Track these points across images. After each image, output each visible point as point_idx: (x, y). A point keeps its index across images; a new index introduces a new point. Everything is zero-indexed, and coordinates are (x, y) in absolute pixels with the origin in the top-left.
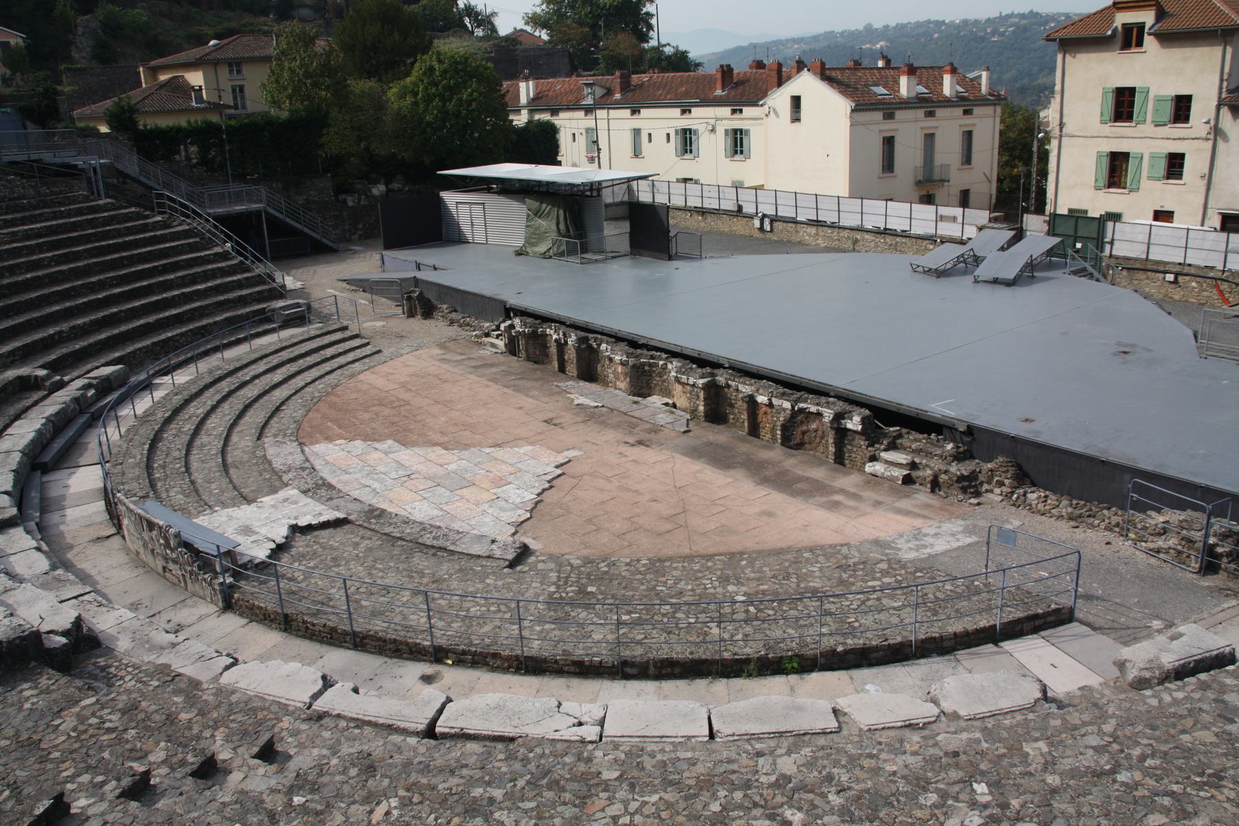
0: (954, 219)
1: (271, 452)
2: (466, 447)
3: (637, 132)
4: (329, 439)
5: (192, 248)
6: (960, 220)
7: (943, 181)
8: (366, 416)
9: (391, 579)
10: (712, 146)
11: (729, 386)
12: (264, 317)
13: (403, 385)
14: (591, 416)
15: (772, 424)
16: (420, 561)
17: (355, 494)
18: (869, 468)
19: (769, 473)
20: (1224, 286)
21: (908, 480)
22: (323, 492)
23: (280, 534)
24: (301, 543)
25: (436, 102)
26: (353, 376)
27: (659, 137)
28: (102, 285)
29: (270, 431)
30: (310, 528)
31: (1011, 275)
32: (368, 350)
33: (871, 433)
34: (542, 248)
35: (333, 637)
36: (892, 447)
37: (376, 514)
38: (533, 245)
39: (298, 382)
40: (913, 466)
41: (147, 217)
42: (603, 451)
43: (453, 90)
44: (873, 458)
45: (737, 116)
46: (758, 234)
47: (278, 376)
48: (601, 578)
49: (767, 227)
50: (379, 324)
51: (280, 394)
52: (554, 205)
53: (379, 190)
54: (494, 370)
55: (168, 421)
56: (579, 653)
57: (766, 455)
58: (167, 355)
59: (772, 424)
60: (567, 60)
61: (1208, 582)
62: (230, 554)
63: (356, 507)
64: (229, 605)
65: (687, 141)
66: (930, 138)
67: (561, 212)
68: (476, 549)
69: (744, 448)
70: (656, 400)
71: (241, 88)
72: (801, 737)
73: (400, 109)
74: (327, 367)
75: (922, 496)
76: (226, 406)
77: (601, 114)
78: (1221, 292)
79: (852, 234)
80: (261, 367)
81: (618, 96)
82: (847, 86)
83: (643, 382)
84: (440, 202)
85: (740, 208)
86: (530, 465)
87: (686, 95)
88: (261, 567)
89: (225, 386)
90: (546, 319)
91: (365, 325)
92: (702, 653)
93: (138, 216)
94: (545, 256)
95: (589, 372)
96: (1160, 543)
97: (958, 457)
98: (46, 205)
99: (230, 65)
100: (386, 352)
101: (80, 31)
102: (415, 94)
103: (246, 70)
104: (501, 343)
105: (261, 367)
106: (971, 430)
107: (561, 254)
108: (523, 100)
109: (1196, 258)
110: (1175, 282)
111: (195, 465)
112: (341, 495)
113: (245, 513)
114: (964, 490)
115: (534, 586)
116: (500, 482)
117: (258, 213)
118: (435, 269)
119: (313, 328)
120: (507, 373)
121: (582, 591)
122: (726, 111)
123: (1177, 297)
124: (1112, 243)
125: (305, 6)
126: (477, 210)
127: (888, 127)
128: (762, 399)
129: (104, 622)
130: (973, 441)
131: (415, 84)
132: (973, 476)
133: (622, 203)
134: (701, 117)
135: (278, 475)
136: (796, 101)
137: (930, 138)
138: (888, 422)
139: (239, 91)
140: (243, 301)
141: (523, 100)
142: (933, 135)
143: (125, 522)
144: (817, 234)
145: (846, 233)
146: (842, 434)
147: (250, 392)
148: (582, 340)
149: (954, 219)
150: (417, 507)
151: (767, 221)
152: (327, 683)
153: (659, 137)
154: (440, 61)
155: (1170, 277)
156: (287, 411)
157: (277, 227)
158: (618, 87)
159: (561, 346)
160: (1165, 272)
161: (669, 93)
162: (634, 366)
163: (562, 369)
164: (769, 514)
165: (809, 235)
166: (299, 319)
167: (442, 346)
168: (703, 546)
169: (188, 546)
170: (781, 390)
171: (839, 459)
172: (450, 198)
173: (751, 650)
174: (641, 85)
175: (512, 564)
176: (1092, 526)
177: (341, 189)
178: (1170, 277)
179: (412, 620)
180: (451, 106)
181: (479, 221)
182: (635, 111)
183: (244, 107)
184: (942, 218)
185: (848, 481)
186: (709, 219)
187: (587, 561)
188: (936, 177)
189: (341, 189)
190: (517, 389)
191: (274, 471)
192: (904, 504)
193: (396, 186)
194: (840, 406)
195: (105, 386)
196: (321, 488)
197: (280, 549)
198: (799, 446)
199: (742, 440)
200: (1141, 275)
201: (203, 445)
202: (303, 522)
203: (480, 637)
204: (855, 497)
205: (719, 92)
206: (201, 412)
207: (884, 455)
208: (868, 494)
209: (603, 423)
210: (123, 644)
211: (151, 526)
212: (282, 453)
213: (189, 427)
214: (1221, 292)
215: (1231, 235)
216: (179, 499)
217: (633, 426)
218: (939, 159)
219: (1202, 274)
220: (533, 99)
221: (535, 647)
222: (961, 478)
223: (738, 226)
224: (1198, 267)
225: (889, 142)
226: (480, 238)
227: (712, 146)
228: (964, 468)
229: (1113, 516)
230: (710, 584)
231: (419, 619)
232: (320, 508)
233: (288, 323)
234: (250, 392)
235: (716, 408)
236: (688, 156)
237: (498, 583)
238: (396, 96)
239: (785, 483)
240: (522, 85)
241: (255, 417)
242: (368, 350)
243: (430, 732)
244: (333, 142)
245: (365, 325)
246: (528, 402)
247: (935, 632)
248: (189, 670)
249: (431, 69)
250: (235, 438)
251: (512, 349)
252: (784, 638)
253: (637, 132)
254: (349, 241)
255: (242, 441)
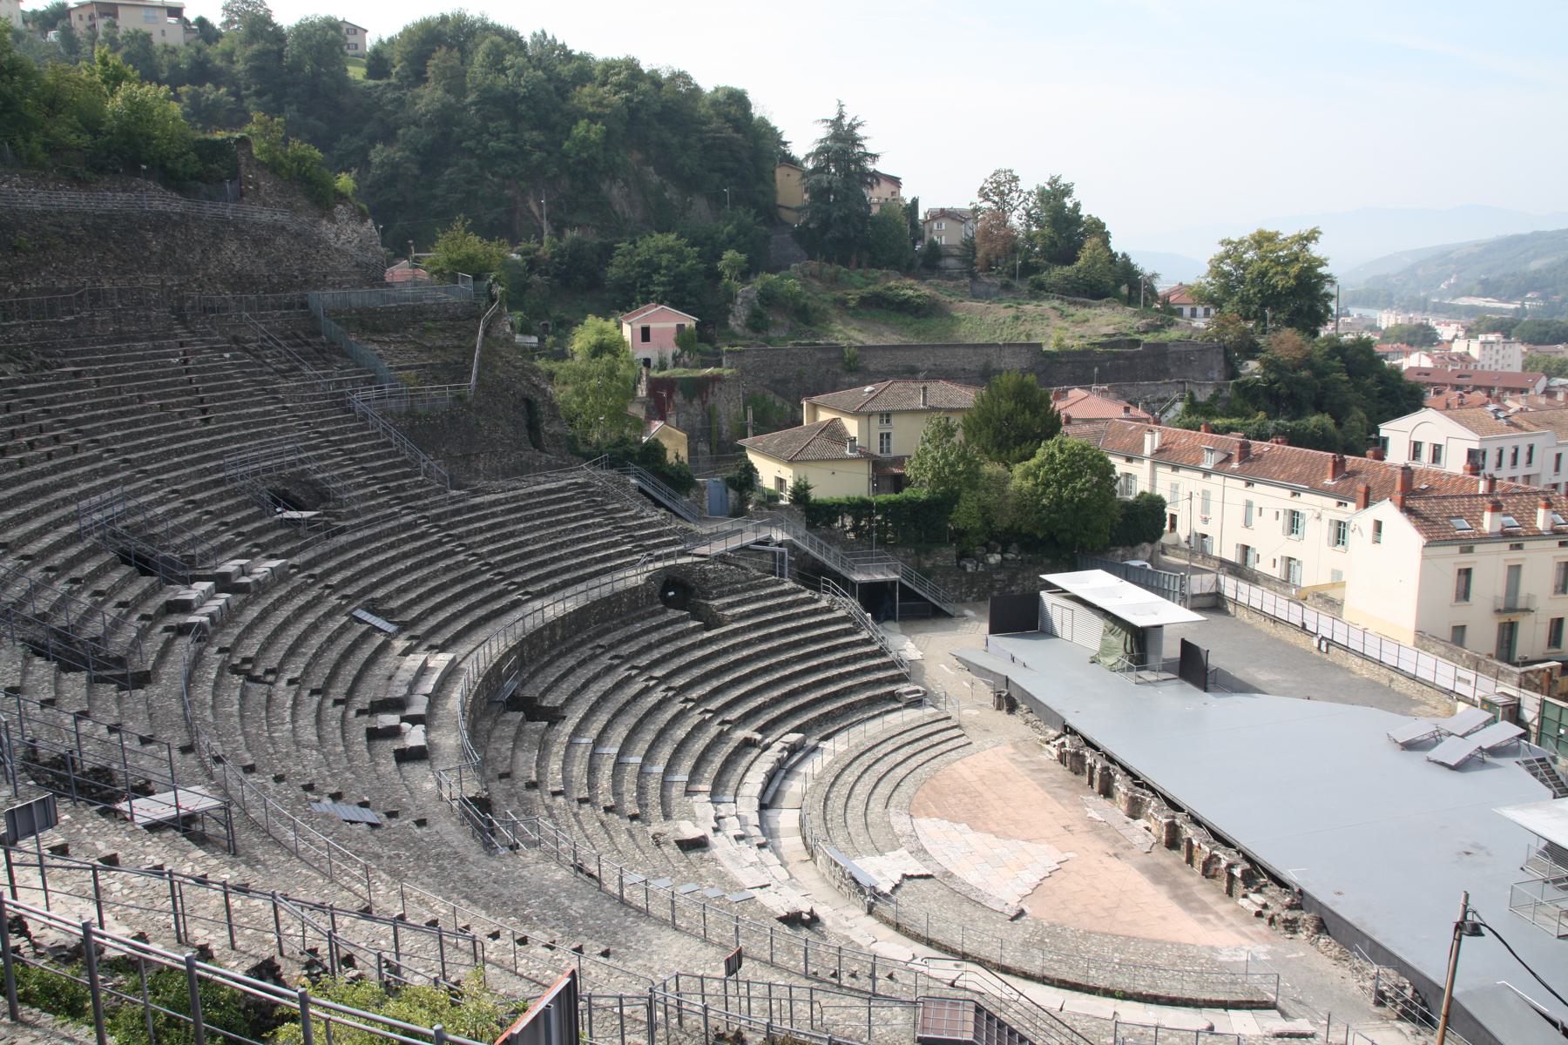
0: (1469, 682)
1: (893, 819)
2: (1010, 837)
3: (1249, 505)
4: (928, 815)
5: (847, 632)
7: (1527, 610)
8: (953, 801)
9: (950, 915)
10: (1316, 532)
12: (893, 697)
13: (981, 778)
14: (1095, 828)
15: (1200, 858)
16: (966, 907)
17: (939, 859)
19: (1180, 892)
21: (1259, 914)
22: (921, 855)
23: (897, 878)
24: (907, 884)
25: (1053, 488)
26: (949, 763)
27: (1269, 514)
28: (787, 663)
29: (893, 802)
30: (911, 877)
31: (1453, 763)
32: (962, 741)
33: (1249, 879)
34: (1111, 660)
35: (917, 938)
36: (1259, 891)
37: (948, 875)
38: (1105, 655)
39: (913, 763)
40: (1265, 906)
41: (817, 601)
42: (1090, 854)
43: (1071, 478)
44: (1245, 896)
45: (1342, 508)
46: (1316, 652)
47: (899, 756)
48: (1055, 936)
49: (1324, 648)
50: (975, 712)
51: (900, 772)
53: (994, 559)
54: (1045, 775)
55: (833, 784)
56: (1026, 968)
57: (1188, 879)
58: (830, 724)
59: (1200, 858)
60: (1221, 357)
62: (873, 888)
63: (938, 868)
64: (870, 912)
65: (1294, 521)
66: (1515, 571)
68: (997, 907)
69: (1177, 871)
70: (1142, 823)
71: (888, 435)
73: (1020, 489)
74: (933, 752)
75: (1262, 925)
76: (866, 776)
77: (1216, 479)
80: (889, 746)
81: (1235, 465)
82: (1426, 519)
83: (1135, 809)
84: (1037, 600)
86: (1044, 857)
87: (1297, 478)
88: (886, 896)
89: (867, 759)
90: (1089, 744)
91: (965, 712)
92: (1081, 981)
93: (811, 601)
94: (1112, 668)
95: (1107, 791)
97: (1290, 907)
98: (752, 588)
99: (882, 415)
100: (975, 745)
101: (739, 300)
102: (1036, 477)
103: (893, 420)
104: (1055, 752)
105: (889, 746)
107: (1122, 670)
108: (1147, 451)
111: (849, 821)
112: (931, 858)
113: (877, 860)
115: (1020, 932)
116: (1022, 867)
117: (893, 583)
119: (927, 712)
120: (1053, 781)
121: (1042, 941)
122: (1333, 502)
125: (953, 256)
126: (1067, 614)
127: (1465, 560)
128: (1195, 842)
129: (819, 911)
130: (1301, 900)
131: (1039, 467)
132: (1295, 921)
133: (1209, 594)
134: (1308, 503)
135: (897, 837)
136: (1378, 526)
137: (1515, 571)
138: (1256, 874)
139: (885, 437)
140: (879, 683)
141: (1147, 451)
142: (1519, 567)
143: (820, 858)
145: (1384, 671)
146: (1231, 877)
147: (881, 768)
148: (1105, 769)
149: (1469, 682)
150: (970, 875)
151: (1324, 643)
152: (914, 957)
153: (1269, 514)
154: (1061, 451)
156: (904, 787)
157: (907, 593)
158: (1236, 457)
159: (1092, 769)
161: (1283, 472)
164: (1164, 918)
166: (917, 703)
167: (1015, 745)
168: (1118, 929)
169: (854, 879)
171: (1230, 892)
172: (1043, 594)
173: (1102, 984)
174: (1259, 456)
175: (1012, 919)
177: (962, 555)
179: (955, 939)
180: (1065, 494)
181: (1068, 623)
182: (1249, 484)
183: (888, 451)
185: (1224, 907)
186: (1279, 627)
187: (1053, 925)
188: (1521, 604)
189: (962, 555)
190: (1056, 797)
191: (894, 834)
192: (1246, 929)
193: (1010, 556)
194: (1237, 858)
195: (793, 749)
196: (920, 852)
197: (897, 886)
198: (1214, 877)
199: (1180, 865)
202: (909, 873)
203: (984, 953)
204: (1221, 918)
205: (1328, 481)
206: (852, 780)
207: (1251, 896)
208: (1230, 919)
209: (1099, 835)
210: (828, 923)
211: (836, 865)
212: (900, 822)
213: (845, 792)
216: (842, 845)
217: (1117, 841)
218: (1526, 588)
220: (1158, 451)
221: (1007, 962)
222: (1286, 921)
223: (1301, 640)
225: (1466, 573)
226: (1067, 636)
227: (1316, 532)
228: (1290, 915)
230: (1107, 951)
231: (958, 938)
232: (918, 865)
233: (910, 705)
234: (881, 768)
235: (1173, 840)
236: (1293, 536)
237: (1003, 928)
238: (1019, 478)
239: (1185, 900)
240: (1148, 437)
241: (884, 789)
242: (962, 741)
243: (952, 985)
244: (964, 515)
245: (965, 712)
246: (1058, 808)
247: (1194, 996)
248: (858, 940)
249: (1052, 455)
250: (872, 805)
251: (1062, 758)
252: (1123, 982)
253: (1249, 505)
254: (963, 601)
255: (876, 807)
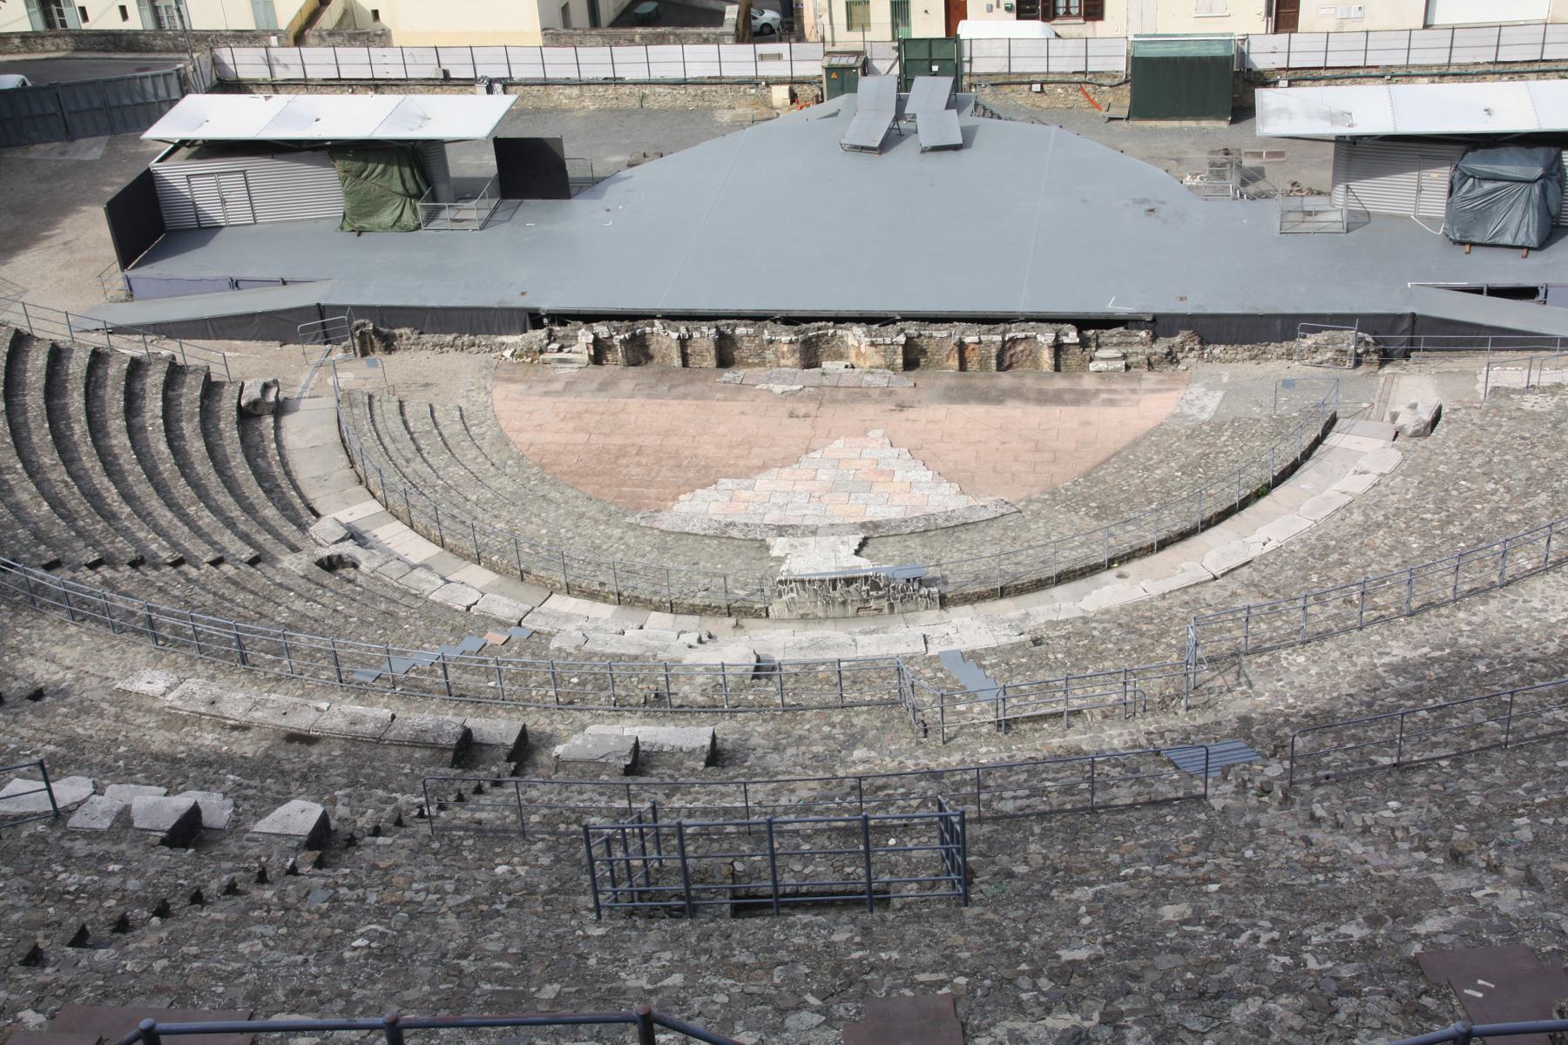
0: (779, 57)
6: (786, 56)
11: (920, 336)
18: (1092, 367)
20: (1089, 88)
52: (389, 163)
61: (1362, 370)
67: (407, 172)
72: (136, 783)
75: (1150, 378)
78: (1086, 95)
79: (636, 89)
85: (446, 73)
96: (1319, 358)
106: (1156, 319)
109: (1057, 66)
110: (1042, 91)
114: (1171, 362)
118: (284, 283)
123: (1044, 105)
124: (970, 61)
130: (1159, 325)
144: (582, 95)
149: (779, 57)
155: (1037, 87)
160: (1031, 83)
162: (804, 342)
163: (57, 355)
165: (570, 98)
170: (985, 327)
176: (1267, 360)
178: (1037, 87)
184: (762, 57)
198: (1010, 366)
200: (1007, 89)
201: (1264, 465)
214: (1086, 95)
215: (1425, 173)
219: (1064, 80)
224: (1061, 73)
229: (1276, 349)
